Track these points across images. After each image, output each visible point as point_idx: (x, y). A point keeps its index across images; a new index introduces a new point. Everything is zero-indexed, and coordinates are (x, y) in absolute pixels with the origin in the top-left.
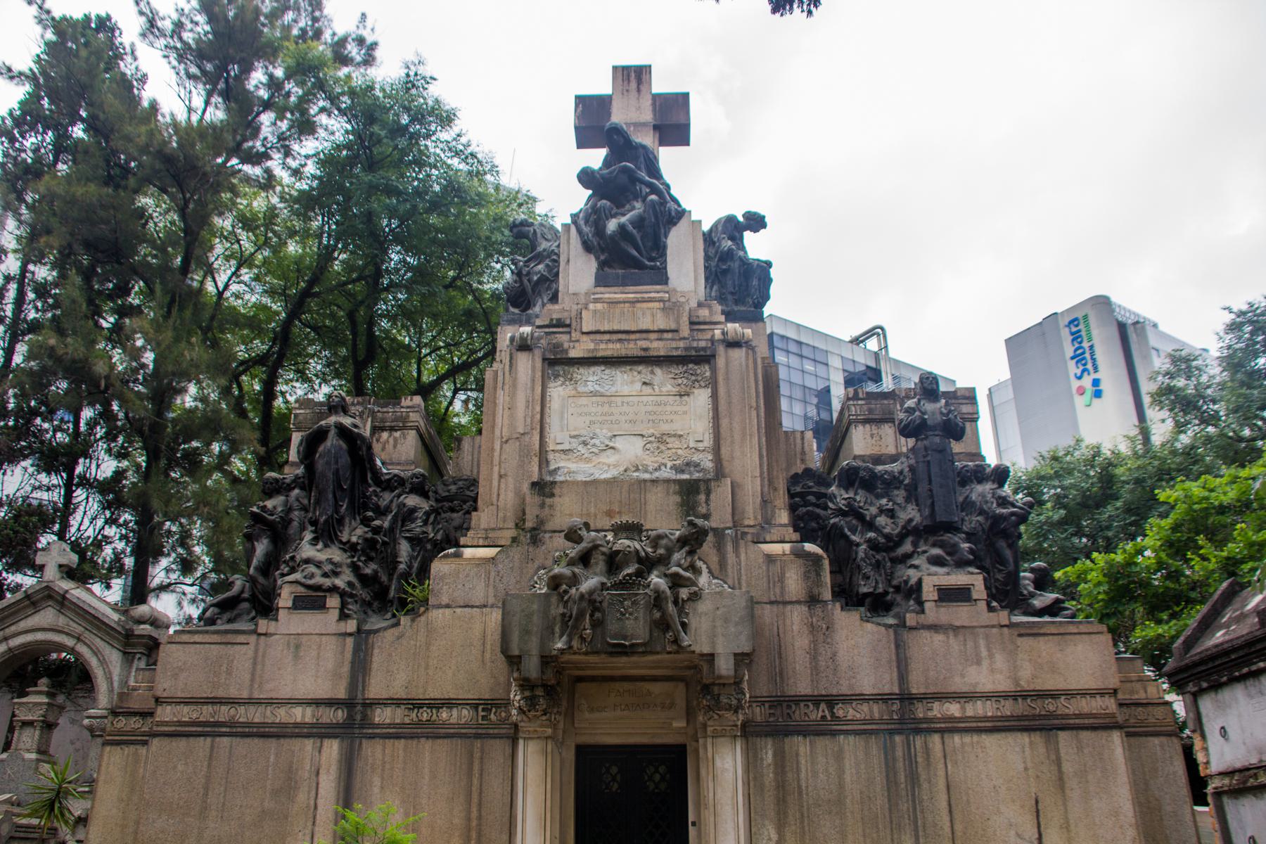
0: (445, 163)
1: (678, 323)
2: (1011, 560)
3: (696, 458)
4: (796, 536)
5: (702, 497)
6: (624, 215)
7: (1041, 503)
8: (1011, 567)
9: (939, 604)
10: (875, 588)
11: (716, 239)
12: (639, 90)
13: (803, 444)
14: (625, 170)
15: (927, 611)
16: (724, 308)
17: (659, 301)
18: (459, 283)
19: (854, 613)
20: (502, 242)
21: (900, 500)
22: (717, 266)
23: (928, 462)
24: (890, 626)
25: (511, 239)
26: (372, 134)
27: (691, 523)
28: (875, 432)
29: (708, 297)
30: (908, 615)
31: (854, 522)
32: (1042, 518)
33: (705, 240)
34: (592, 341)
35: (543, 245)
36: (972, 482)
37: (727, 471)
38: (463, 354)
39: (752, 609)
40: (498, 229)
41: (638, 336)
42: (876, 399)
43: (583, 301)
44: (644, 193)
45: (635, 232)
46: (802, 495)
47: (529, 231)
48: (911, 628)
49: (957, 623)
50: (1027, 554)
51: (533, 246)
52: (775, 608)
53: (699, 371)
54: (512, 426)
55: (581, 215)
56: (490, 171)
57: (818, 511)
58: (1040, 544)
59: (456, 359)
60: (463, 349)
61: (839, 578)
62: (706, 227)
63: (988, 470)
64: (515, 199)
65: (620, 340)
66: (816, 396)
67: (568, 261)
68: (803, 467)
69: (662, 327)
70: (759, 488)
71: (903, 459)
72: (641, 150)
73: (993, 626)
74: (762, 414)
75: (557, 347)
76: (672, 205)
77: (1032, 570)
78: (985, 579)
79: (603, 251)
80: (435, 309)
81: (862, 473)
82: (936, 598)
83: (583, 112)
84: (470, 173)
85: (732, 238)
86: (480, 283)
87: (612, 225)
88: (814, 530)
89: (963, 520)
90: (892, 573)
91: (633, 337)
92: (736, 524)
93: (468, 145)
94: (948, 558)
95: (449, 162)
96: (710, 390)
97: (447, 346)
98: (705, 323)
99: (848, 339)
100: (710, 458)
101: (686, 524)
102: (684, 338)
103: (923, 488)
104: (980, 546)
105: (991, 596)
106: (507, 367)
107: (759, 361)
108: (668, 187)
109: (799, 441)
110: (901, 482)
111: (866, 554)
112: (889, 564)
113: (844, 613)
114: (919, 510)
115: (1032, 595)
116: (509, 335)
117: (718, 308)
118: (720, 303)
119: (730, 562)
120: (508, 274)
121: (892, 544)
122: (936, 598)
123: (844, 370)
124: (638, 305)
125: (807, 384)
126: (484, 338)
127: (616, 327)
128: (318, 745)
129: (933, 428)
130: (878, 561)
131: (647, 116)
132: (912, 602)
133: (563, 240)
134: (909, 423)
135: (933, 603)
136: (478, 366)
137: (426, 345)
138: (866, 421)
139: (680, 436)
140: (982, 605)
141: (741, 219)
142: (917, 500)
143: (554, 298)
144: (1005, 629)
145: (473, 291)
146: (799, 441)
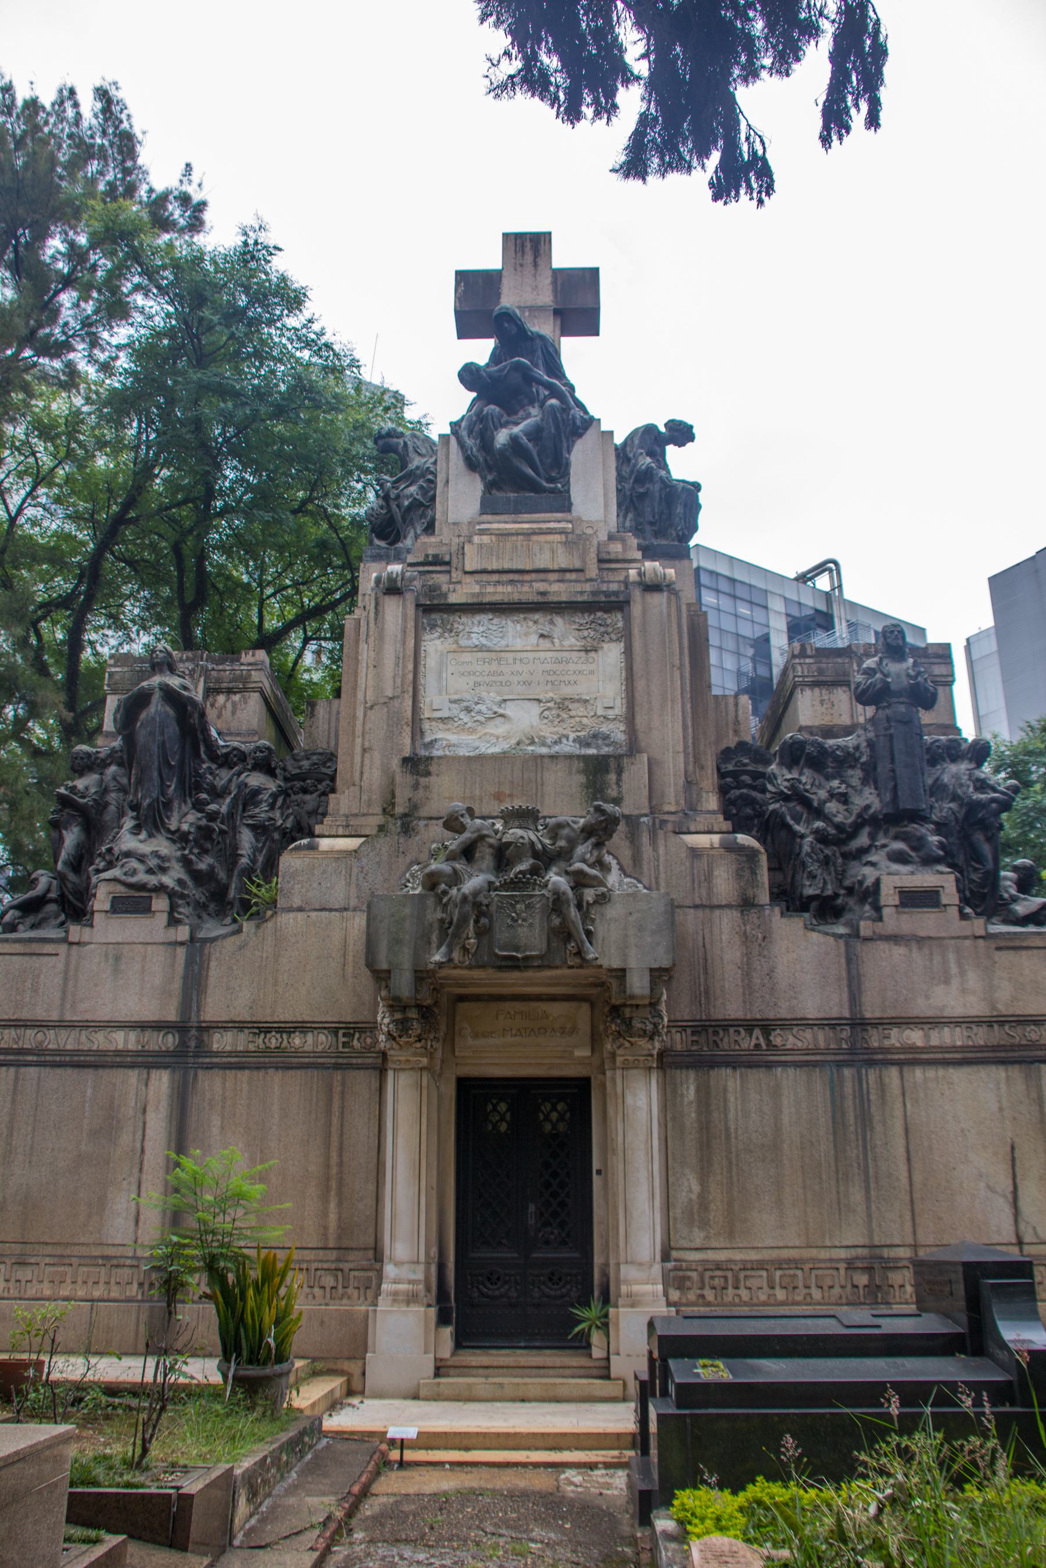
0: (292, 356)
1: (584, 561)
2: (990, 857)
3: (604, 729)
4: (727, 826)
5: (612, 777)
6: (517, 424)
7: (1028, 784)
8: (990, 865)
9: (900, 909)
10: (823, 889)
11: (631, 455)
12: (535, 265)
13: (736, 711)
14: (518, 367)
15: (885, 918)
16: (641, 541)
17: (560, 533)
18: (310, 507)
19: (796, 920)
20: (364, 455)
21: (855, 782)
22: (633, 488)
23: (891, 736)
24: (841, 936)
25: (375, 453)
26: (201, 320)
27: (599, 810)
28: (826, 697)
29: (621, 528)
30: (862, 923)
31: (798, 808)
32: (1029, 802)
33: (618, 456)
34: (477, 582)
35: (416, 462)
36: (944, 760)
37: (643, 744)
38: (315, 595)
39: (673, 914)
40: (359, 439)
41: (534, 576)
42: (828, 657)
43: (465, 532)
44: (542, 397)
45: (530, 445)
46: (735, 774)
47: (398, 444)
48: (867, 939)
49: (922, 933)
50: (1009, 847)
51: (404, 463)
52: (700, 913)
53: (609, 621)
54: (378, 688)
55: (463, 424)
56: (350, 366)
57: (754, 794)
58: (1024, 834)
59: (306, 600)
60: (315, 589)
61: (779, 877)
62: (619, 439)
63: (964, 746)
64: (380, 401)
65: (512, 582)
66: (752, 646)
67: (447, 482)
68: (736, 739)
69: (563, 566)
70: (682, 766)
71: (860, 732)
72: (538, 341)
73: (966, 938)
74: (687, 675)
75: (433, 590)
76: (577, 412)
77: (1015, 869)
78: (957, 880)
79: (490, 469)
80: (280, 540)
81: (809, 749)
82: (897, 903)
83: (464, 292)
84: (325, 368)
85: (651, 454)
86: (337, 507)
87: (502, 437)
88: (749, 818)
89: (932, 807)
90: (844, 871)
91: (527, 577)
92: (653, 810)
93: (321, 334)
94: (913, 854)
95: (298, 354)
96: (622, 644)
97: (296, 584)
98: (618, 561)
99: (793, 576)
100: (622, 728)
101: (592, 809)
102: (591, 580)
103: (883, 768)
104: (951, 840)
105: (965, 901)
106: (372, 615)
107: (684, 608)
108: (572, 388)
109: (731, 708)
110: (857, 760)
111: (812, 848)
112: (840, 860)
113: (784, 920)
114: (878, 795)
115: (1014, 899)
116: (374, 575)
117: (633, 541)
118: (636, 536)
119: (645, 856)
120: (371, 495)
121: (843, 836)
122: (897, 903)
123: (787, 615)
124: (535, 538)
125: (741, 632)
126: (341, 575)
127: (507, 566)
128: (145, 1076)
129: (899, 694)
130: (826, 857)
131: (546, 297)
132: (867, 907)
133: (441, 455)
134: (868, 688)
135: (893, 909)
136: (333, 610)
137: (269, 583)
138: (815, 684)
139: (586, 701)
140: (954, 912)
141: (663, 429)
142: (875, 782)
143: (430, 528)
144: (981, 942)
145: (327, 517)
146: (731, 708)
